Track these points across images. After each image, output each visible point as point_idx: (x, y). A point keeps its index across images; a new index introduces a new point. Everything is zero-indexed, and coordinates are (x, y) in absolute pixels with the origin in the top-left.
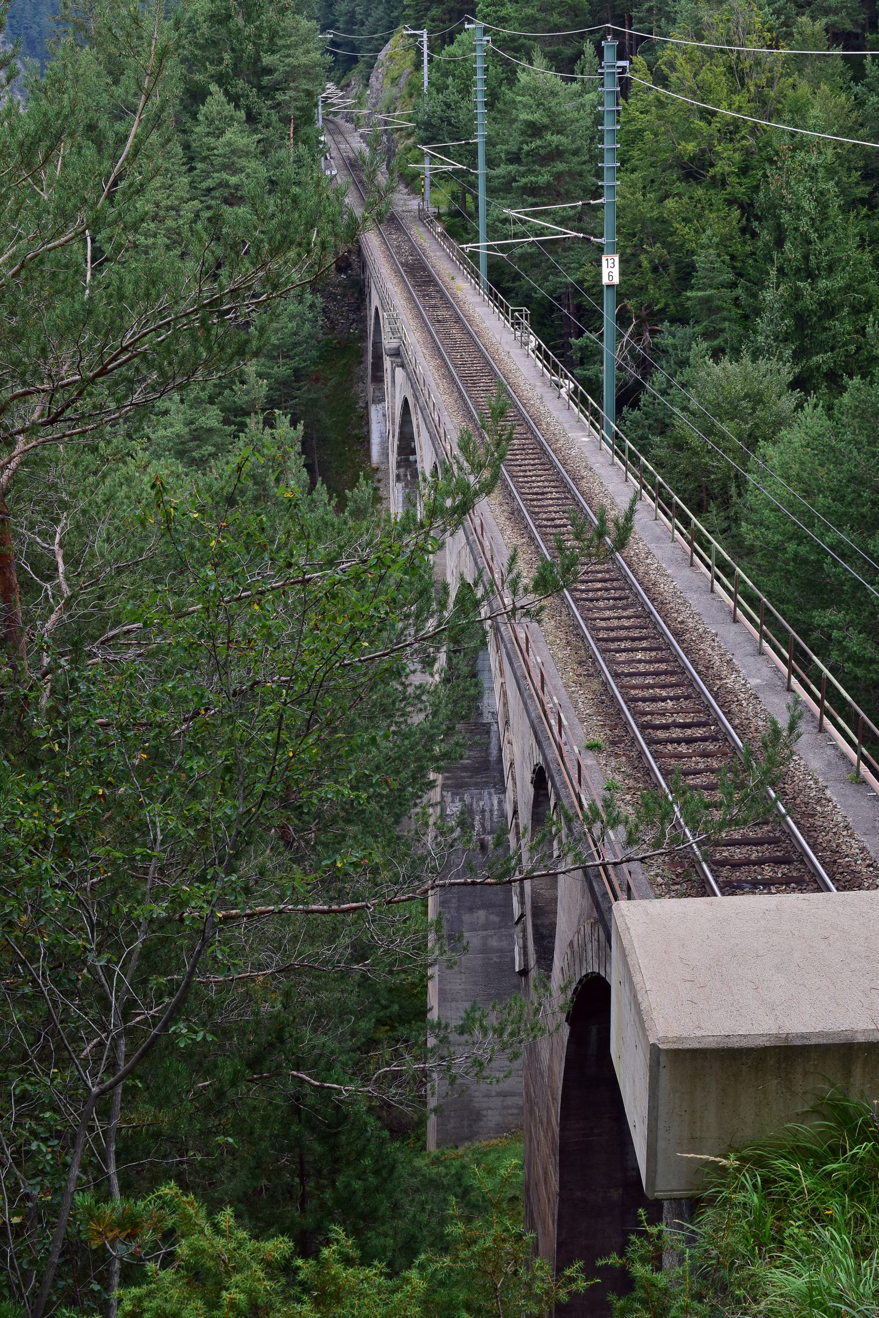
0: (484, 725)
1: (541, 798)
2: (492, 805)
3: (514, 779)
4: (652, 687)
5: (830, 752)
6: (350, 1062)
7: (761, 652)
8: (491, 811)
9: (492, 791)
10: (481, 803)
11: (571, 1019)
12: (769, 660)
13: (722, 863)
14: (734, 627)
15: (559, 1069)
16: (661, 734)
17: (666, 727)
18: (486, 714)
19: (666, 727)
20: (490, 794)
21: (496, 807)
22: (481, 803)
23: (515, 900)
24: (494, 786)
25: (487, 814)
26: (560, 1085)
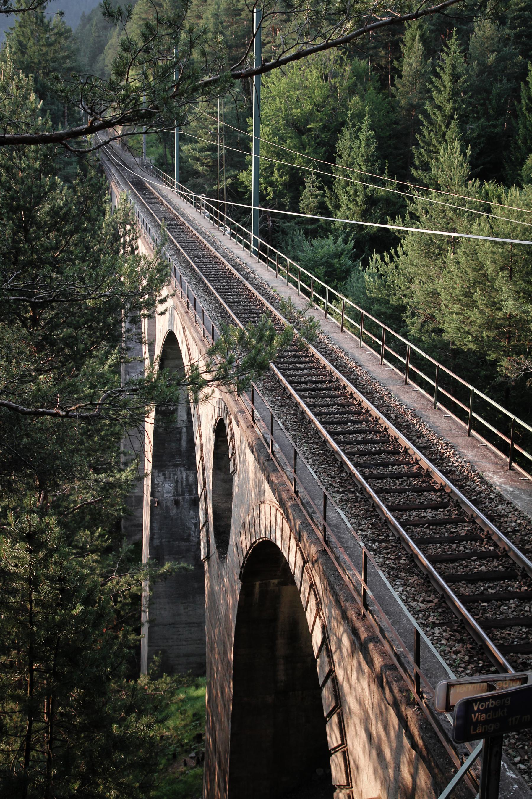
0: (177, 428)
1: (220, 443)
2: (182, 478)
3: (200, 436)
4: (294, 363)
5: (414, 395)
6: (36, 194)
7: (361, 346)
8: (182, 482)
9: (183, 469)
10: (176, 477)
11: (242, 577)
12: (366, 350)
13: (353, 454)
14: (342, 334)
15: (232, 616)
16: (303, 386)
17: (306, 383)
18: (179, 421)
19: (306, 383)
20: (181, 471)
21: (184, 479)
22: (176, 477)
23: (201, 513)
24: (184, 466)
25: (179, 484)
26: (233, 625)
